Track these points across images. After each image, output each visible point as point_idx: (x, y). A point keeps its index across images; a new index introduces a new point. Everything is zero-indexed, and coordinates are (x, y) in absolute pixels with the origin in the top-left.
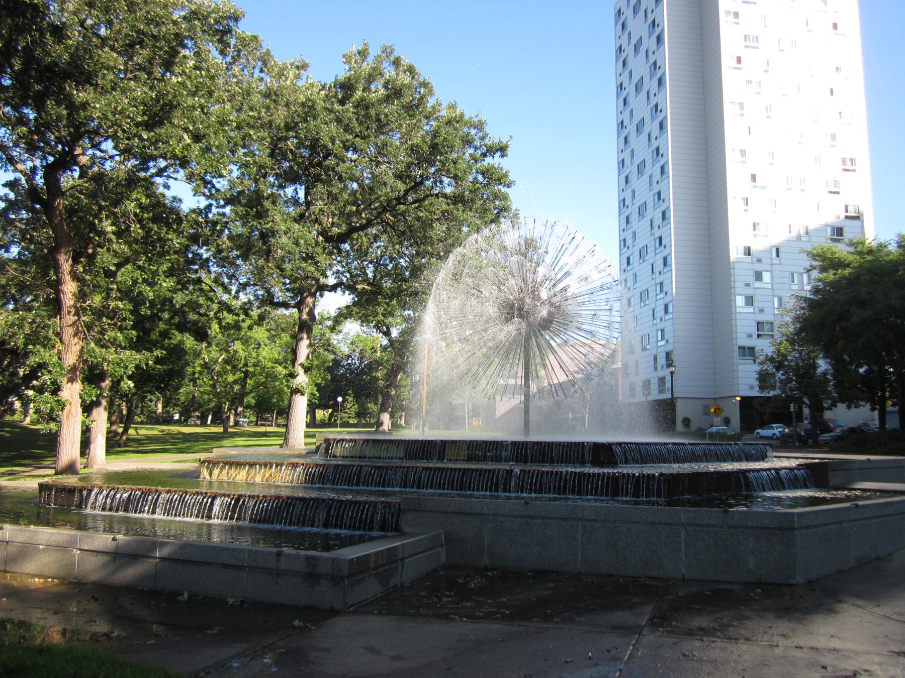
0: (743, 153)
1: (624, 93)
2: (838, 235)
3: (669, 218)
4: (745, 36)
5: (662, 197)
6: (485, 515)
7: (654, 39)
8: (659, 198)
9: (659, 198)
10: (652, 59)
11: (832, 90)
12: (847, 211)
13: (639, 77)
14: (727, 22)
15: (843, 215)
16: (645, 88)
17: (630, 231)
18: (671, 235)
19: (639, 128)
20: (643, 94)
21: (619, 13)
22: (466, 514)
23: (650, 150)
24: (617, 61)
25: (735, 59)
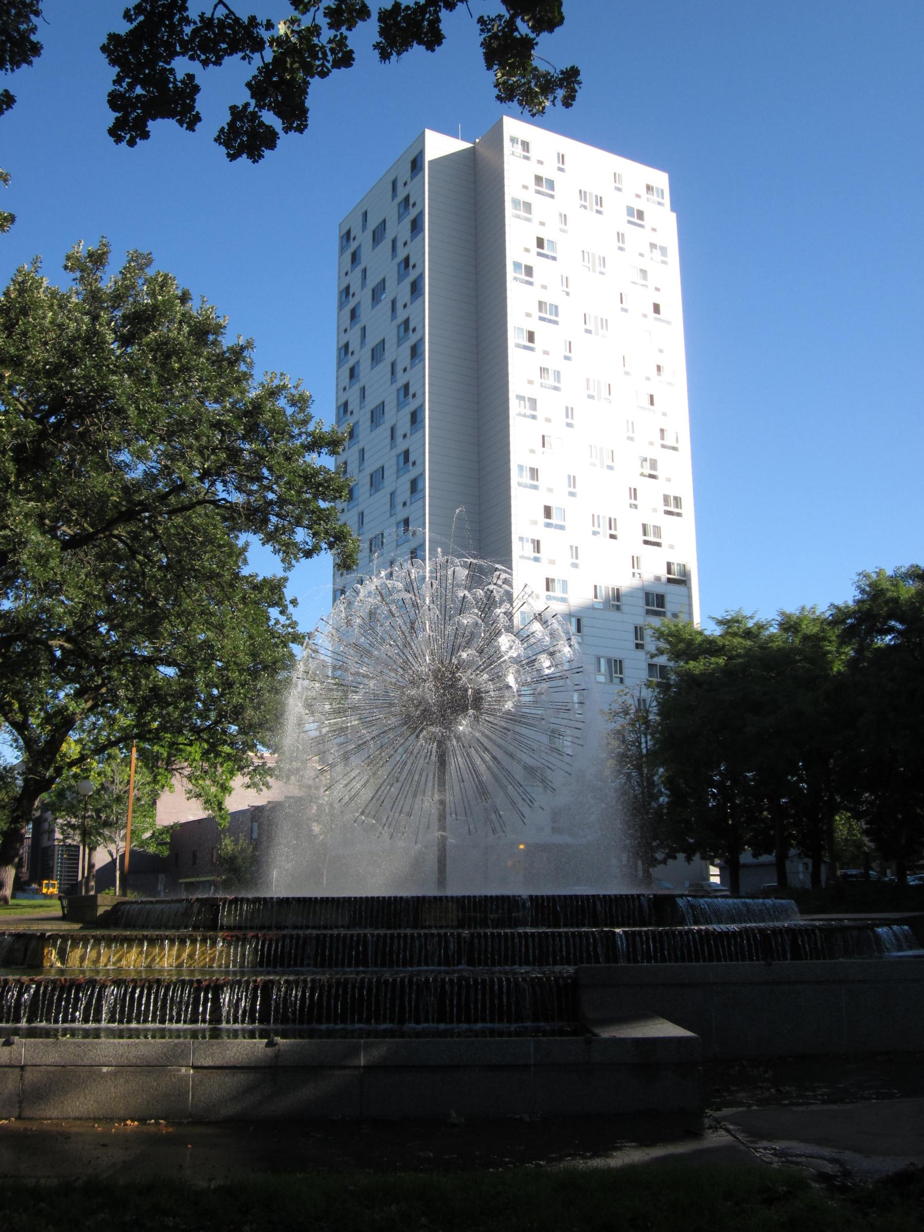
0: (534, 473)
1: (352, 361)
2: (658, 606)
4: (540, 303)
7: (407, 221)
10: (402, 315)
11: (652, 397)
12: (669, 572)
13: (380, 220)
14: (515, 279)
15: (663, 574)
16: (389, 235)
17: (357, 388)
19: (377, 354)
20: (385, 366)
21: (347, 236)
23: (393, 520)
24: (341, 306)
25: (526, 335)
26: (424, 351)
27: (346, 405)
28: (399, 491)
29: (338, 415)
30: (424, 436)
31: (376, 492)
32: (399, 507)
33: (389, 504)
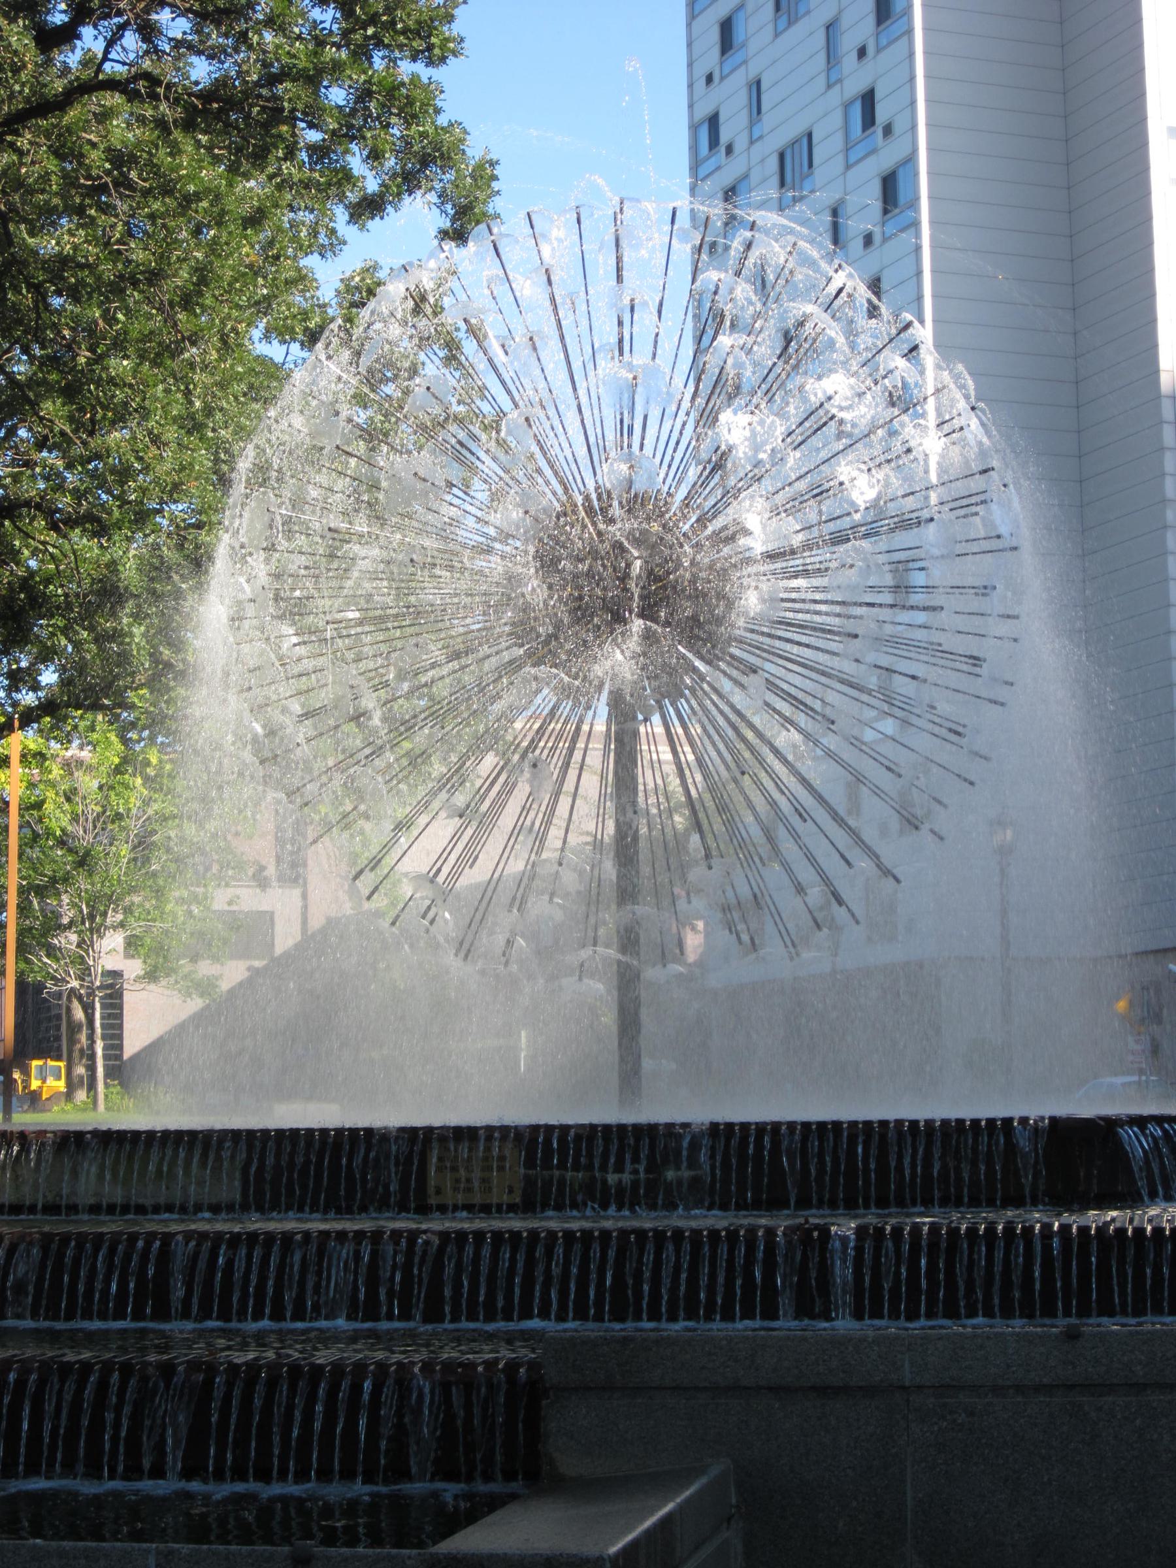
3: (914, 203)
5: (881, 116)
6: (903, 1388)
7: (870, 171)
8: (869, 119)
9: (869, 119)
17: (737, 82)
18: (919, 273)
22: (823, 1391)
23: (835, 97)
26: (917, 198)
27: (713, 121)
28: (846, 21)
29: (694, 148)
30: (911, 55)
31: (790, 24)
32: (849, 60)
33: (822, 56)
